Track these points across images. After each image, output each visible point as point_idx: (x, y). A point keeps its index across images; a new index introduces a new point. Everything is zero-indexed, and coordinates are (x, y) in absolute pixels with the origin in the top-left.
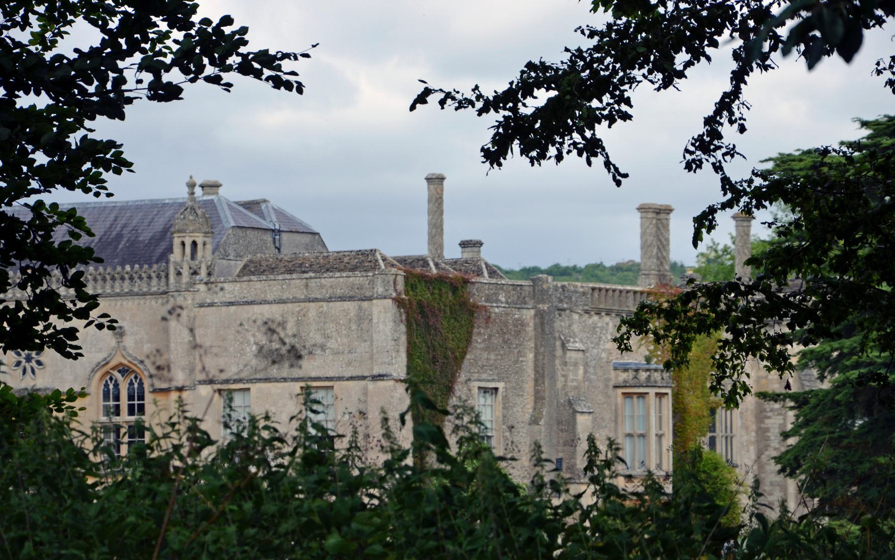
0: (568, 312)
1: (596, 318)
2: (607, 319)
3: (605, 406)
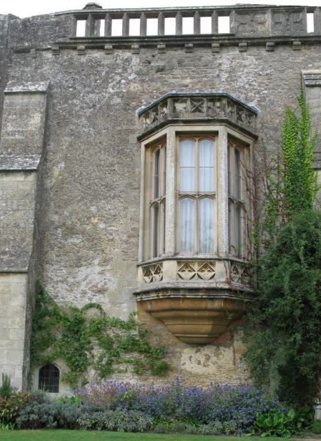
0: (33, 51)
1: (97, 54)
2: (127, 54)
3: (116, 167)
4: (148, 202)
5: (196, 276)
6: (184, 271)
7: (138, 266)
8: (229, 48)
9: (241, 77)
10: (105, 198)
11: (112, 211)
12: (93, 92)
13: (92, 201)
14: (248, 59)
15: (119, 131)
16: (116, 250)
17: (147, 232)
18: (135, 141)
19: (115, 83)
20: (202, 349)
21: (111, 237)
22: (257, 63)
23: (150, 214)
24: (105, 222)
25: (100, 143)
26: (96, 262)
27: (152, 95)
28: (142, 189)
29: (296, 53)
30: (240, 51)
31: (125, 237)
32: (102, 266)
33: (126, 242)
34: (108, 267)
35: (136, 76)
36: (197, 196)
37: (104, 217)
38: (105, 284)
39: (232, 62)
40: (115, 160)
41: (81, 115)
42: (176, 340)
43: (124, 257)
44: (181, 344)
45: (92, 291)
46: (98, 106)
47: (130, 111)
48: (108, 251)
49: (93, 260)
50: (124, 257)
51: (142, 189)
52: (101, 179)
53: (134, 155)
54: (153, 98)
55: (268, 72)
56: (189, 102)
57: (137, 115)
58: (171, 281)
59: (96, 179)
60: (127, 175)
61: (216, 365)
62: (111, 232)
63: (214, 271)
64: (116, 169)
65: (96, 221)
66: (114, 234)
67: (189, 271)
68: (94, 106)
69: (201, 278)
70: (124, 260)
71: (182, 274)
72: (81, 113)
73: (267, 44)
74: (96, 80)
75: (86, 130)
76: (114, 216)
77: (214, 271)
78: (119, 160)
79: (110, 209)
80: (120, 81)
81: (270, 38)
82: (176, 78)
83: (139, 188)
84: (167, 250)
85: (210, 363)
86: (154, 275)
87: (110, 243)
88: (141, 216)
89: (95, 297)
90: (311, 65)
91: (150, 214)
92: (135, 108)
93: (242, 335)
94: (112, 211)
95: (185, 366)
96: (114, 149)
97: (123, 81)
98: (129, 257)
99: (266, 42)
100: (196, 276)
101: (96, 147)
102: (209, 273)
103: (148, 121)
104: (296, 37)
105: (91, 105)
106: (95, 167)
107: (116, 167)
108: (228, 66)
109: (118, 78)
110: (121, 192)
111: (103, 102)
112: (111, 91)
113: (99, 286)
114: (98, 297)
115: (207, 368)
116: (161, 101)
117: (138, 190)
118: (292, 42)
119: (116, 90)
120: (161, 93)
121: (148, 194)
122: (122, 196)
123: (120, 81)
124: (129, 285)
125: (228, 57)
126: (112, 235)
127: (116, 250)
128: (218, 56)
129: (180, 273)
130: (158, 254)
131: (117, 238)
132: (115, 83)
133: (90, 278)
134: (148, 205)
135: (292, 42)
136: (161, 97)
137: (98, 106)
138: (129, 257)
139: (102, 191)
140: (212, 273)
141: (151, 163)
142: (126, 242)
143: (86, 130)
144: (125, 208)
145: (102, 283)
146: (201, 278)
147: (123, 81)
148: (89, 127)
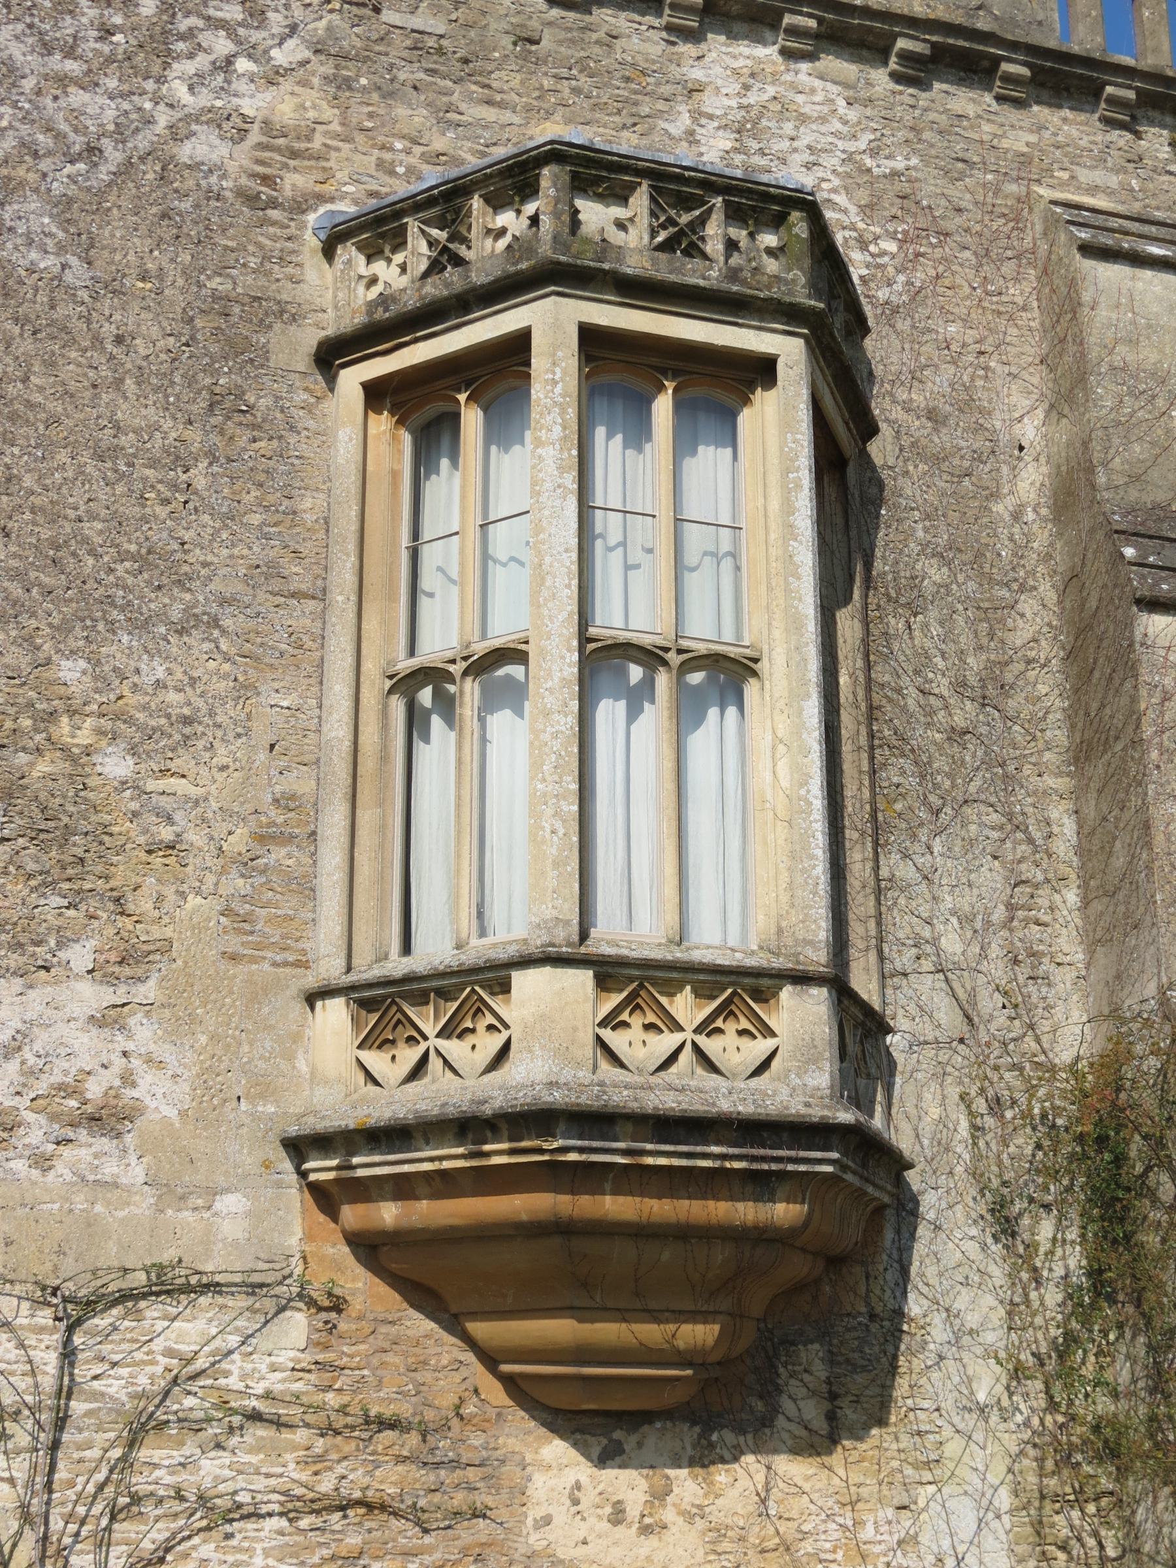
3: (199, 476)
4: (370, 666)
5: (687, 1055)
6: (625, 1025)
7: (312, 998)
8: (737, 27)
9: (784, 162)
10: (141, 625)
11: (173, 697)
12: (89, 83)
13: (63, 629)
14: (813, 91)
15: (216, 297)
16: (193, 901)
17: (367, 817)
18: (303, 360)
19: (202, 61)
20: (630, 1442)
21: (166, 833)
22: (852, 115)
23: (385, 727)
24: (133, 751)
25: (119, 340)
26: (80, 956)
27: (388, 156)
28: (342, 598)
29: (1011, 114)
30: (786, 53)
31: (238, 842)
32: (111, 980)
33: (247, 864)
34: (148, 991)
35: (307, 54)
36: (671, 656)
37: (130, 721)
38: (128, 1079)
39: (747, 87)
40: (194, 435)
41: (22, 184)
42: (495, 1393)
43: (234, 943)
44: (519, 1418)
45: (54, 1117)
46: (114, 156)
47: (274, 214)
48: (147, 906)
49: (60, 945)
50: (234, 943)
51: (342, 598)
52: (119, 522)
53: (292, 428)
54: (392, 173)
55: (899, 164)
56: (640, 200)
57: (312, 242)
58: (567, 1075)
59: (94, 517)
60: (256, 519)
61: (700, 1524)
62: (164, 801)
63: (769, 1032)
64: (200, 483)
65: (84, 737)
66: (178, 816)
67: (649, 1027)
68: (92, 151)
69: (377, 1083)
70: (234, 958)
71: (616, 1039)
72: (21, 172)
73: (901, 44)
74: (107, 32)
75: (49, 262)
76: (187, 721)
77: (769, 1032)
78: (214, 438)
79: (159, 685)
80: (229, 61)
81: (912, 22)
82: (501, 105)
83: (321, 595)
84: (497, 915)
85: (669, 1515)
86: (434, 1042)
87: (157, 861)
88: (337, 729)
89: (66, 1151)
90: (1065, 175)
91: (385, 727)
92: (300, 206)
93: (820, 1370)
94: (173, 697)
95: (552, 1534)
96: (191, 381)
97: (243, 65)
98: (259, 947)
99: (894, 37)
100: (687, 1055)
101: (96, 357)
102: (745, 1042)
103: (387, 273)
104: (1014, 46)
105: (78, 143)
106: (85, 457)
107: (199, 476)
108: (734, 103)
109: (222, 45)
110: (224, 602)
111: (142, 142)
112: (180, 91)
113: (94, 1089)
114: (84, 1153)
115: (653, 1541)
116: (500, 172)
117: (311, 605)
118: (997, 60)
119: (204, 99)
120: (435, 158)
121: (371, 625)
122: (227, 623)
123: (229, 61)
124: (263, 1088)
125: (729, 61)
126: (170, 820)
127: (193, 901)
128: (687, 49)
129: (607, 1034)
130: (490, 930)
131: (195, 837)
132: (202, 61)
133: (42, 1040)
134: (374, 686)
135: (996, 61)
136: (432, 177)
137: (114, 156)
138: (259, 947)
139: (119, 584)
140: (763, 1046)
141: (395, 475)
142: (247, 864)
143: (49, 262)
144: (244, 690)
145: (110, 1078)
146: (377, 1083)
147: (243, 65)
148: (61, 249)
